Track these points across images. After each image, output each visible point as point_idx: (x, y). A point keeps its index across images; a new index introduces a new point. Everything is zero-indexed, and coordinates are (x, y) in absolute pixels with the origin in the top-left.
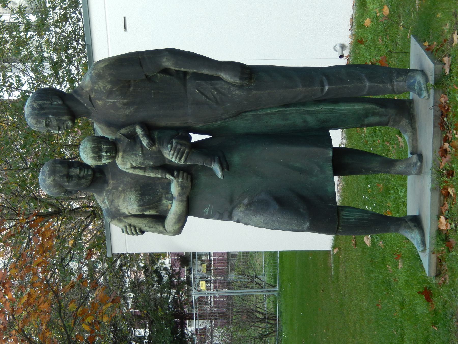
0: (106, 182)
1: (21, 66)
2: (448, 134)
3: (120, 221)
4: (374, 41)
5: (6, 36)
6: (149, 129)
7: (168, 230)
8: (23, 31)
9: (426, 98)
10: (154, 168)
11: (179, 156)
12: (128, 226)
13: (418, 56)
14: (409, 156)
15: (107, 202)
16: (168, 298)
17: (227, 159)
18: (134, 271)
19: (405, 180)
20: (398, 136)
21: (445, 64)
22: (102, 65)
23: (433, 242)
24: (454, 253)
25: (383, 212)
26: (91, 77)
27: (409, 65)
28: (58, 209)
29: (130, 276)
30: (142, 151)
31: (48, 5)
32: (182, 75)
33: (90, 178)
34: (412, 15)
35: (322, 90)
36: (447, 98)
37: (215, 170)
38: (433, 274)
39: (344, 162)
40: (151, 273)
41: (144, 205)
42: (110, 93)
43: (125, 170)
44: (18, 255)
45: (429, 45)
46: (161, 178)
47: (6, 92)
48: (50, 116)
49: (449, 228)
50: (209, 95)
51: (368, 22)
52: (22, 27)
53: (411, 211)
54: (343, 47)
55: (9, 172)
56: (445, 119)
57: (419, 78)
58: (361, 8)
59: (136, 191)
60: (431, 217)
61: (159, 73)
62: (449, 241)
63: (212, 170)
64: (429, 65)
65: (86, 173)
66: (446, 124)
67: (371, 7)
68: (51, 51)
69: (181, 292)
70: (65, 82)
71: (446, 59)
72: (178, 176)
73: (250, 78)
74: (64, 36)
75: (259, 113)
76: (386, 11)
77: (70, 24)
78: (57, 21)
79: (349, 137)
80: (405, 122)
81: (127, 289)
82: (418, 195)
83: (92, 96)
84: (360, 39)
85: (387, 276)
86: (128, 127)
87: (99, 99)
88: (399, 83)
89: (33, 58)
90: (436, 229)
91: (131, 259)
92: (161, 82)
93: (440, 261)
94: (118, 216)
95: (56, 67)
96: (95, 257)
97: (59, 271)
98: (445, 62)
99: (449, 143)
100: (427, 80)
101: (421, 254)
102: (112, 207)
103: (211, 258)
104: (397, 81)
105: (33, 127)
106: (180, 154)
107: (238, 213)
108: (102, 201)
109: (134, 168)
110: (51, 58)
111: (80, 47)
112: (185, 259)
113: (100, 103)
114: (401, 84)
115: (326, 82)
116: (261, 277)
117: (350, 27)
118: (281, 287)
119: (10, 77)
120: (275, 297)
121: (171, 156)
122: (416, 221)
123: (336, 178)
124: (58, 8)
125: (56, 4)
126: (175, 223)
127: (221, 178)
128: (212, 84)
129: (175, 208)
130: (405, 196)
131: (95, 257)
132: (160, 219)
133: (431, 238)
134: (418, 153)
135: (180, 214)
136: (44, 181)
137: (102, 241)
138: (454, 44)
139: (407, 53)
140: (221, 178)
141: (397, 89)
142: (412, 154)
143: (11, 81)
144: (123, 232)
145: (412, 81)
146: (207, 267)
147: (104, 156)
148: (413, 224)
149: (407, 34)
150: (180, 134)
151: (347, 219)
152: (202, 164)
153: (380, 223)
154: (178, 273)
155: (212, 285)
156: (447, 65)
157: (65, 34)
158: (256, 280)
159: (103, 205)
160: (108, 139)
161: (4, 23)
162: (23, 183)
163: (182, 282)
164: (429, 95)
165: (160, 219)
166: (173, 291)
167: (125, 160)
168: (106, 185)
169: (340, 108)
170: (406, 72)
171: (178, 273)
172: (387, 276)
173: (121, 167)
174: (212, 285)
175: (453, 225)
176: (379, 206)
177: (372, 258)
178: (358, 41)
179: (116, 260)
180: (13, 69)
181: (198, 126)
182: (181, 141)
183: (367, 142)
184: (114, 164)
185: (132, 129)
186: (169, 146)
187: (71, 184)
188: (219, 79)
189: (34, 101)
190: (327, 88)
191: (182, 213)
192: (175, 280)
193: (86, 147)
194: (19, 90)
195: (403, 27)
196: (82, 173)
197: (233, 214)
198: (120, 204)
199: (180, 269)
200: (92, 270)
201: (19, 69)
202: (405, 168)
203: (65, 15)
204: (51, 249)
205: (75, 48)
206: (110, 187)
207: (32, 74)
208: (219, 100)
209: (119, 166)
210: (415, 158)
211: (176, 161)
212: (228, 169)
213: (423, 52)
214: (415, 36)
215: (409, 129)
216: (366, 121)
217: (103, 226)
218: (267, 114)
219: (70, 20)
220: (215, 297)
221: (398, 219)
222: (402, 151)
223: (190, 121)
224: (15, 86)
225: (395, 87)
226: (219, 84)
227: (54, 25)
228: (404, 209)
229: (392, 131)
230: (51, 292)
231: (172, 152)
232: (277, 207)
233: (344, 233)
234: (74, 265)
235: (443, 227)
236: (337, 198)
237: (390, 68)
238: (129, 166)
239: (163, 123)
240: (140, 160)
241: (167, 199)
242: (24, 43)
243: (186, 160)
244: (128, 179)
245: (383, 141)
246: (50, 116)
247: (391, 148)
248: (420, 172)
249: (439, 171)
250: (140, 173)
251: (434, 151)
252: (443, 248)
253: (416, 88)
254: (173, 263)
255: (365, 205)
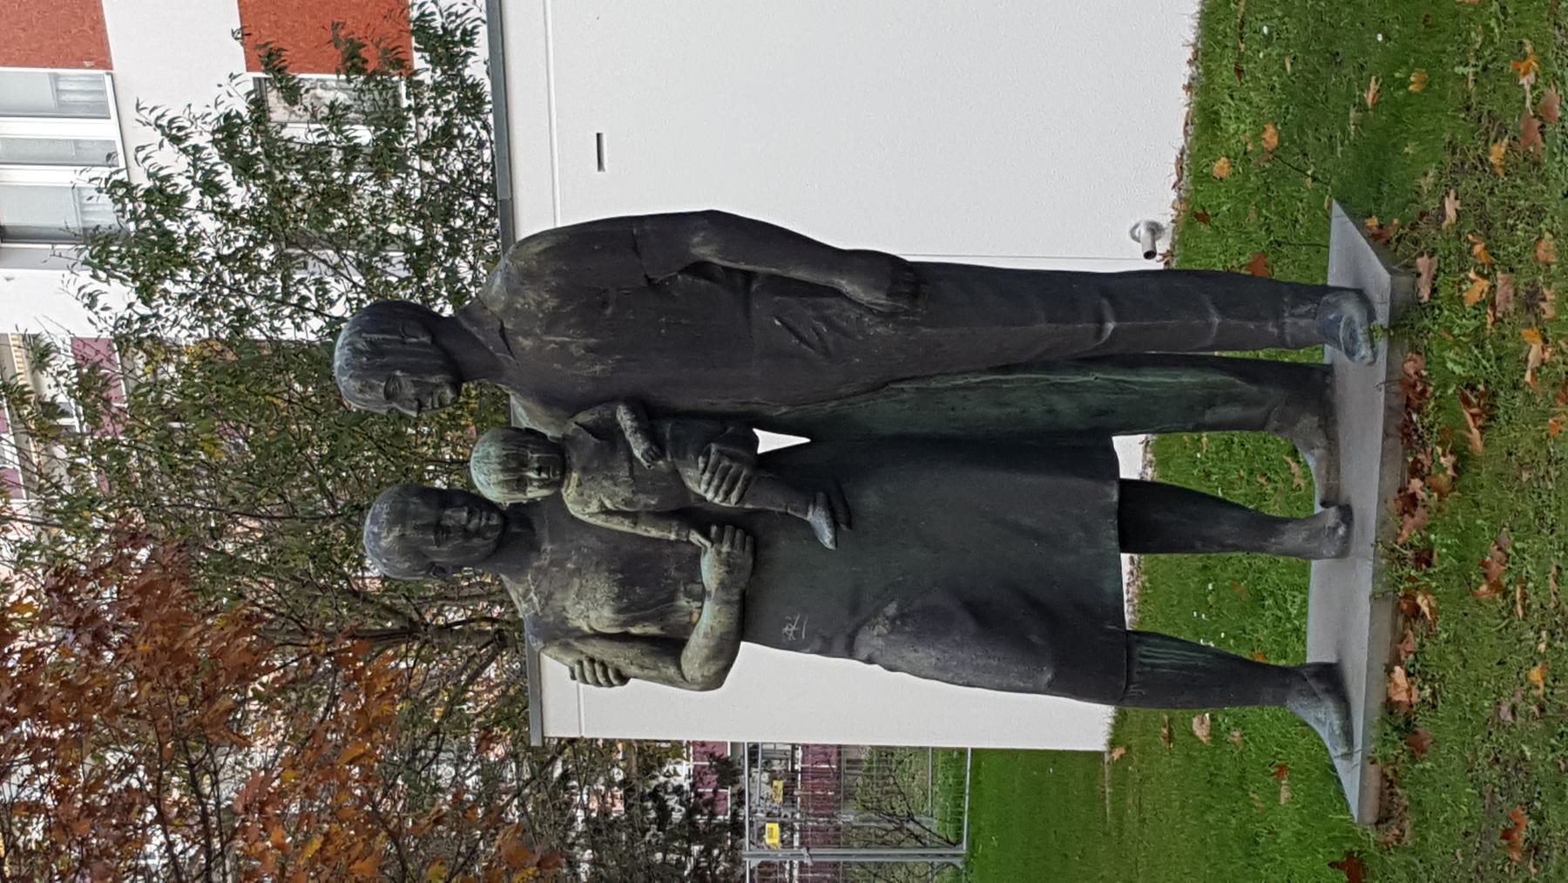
0: (535, 547)
1: (330, 253)
2: (1420, 456)
3: (566, 647)
4: (1233, 213)
5: (293, 176)
6: (649, 415)
7: (689, 678)
8: (339, 166)
9: (1369, 359)
10: (660, 516)
11: (724, 487)
12: (585, 663)
13: (1348, 254)
14: (1318, 509)
15: (535, 599)
16: (680, 865)
17: (849, 500)
18: (597, 792)
19: (1305, 573)
20: (1289, 459)
21: (1419, 275)
22: (536, 248)
23: (1374, 733)
24: (1428, 765)
25: (1245, 654)
26: (507, 279)
27: (1325, 278)
28: (411, 620)
29: (585, 803)
30: (631, 470)
31: (405, 103)
32: (739, 280)
33: (492, 535)
34: (1339, 149)
35: (1100, 331)
36: (1421, 362)
37: (817, 527)
38: (1370, 818)
39: (1147, 517)
40: (643, 798)
41: (629, 608)
42: (552, 322)
43: (585, 518)
44: (303, 736)
45: (1380, 227)
46: (677, 541)
47: (288, 321)
48: (398, 373)
49: (1415, 699)
50: (808, 334)
51: (1221, 167)
52: (337, 157)
53: (1317, 652)
54: (1155, 230)
55: (288, 524)
56: (1415, 417)
57: (1351, 310)
58: (1205, 131)
59: (611, 572)
60: (1369, 669)
61: (680, 272)
62: (1416, 733)
63: (807, 525)
64: (1379, 277)
65: (484, 522)
66: (1416, 430)
67: (1232, 128)
68: (408, 218)
69: (716, 852)
70: (440, 301)
71: (1422, 263)
72: (719, 540)
73: (914, 296)
74: (441, 183)
75: (934, 384)
76: (1271, 137)
77: (459, 153)
78: (426, 144)
79: (1161, 458)
80: (1309, 421)
81: (578, 837)
82: (1338, 612)
83: (508, 326)
84: (1200, 211)
85: (1248, 821)
86: (599, 408)
87: (526, 336)
88: (1297, 322)
89: (361, 237)
90: (1384, 699)
91: (590, 755)
92: (683, 288)
93: (1389, 783)
94: (561, 635)
95: (420, 259)
96: (500, 750)
97: (405, 781)
98: (1421, 270)
99: (1422, 479)
100: (1371, 316)
101: (1339, 764)
102: (548, 611)
103: (798, 767)
104: (1292, 315)
105: (354, 399)
106: (727, 481)
107: (871, 638)
108: (524, 599)
109: (608, 512)
110: (406, 238)
111: (482, 212)
112: (724, 766)
113: (527, 343)
114: (1303, 322)
115: (1108, 312)
116: (923, 819)
117: (1174, 178)
118: (972, 846)
119: (301, 281)
120: (957, 873)
121: (703, 487)
122: (1330, 678)
123: (1125, 557)
124: (430, 110)
125: (426, 101)
126: (708, 659)
127: (831, 547)
128: (815, 307)
129: (709, 619)
130: (1303, 614)
131: (500, 750)
132: (669, 646)
133: (1368, 724)
134: (1342, 502)
135: (721, 638)
136: (377, 537)
137: (519, 705)
138: (1444, 225)
139: (1321, 249)
140: (831, 547)
141: (1293, 337)
142: (1324, 504)
143: (304, 292)
144: (573, 677)
145: (1331, 317)
146: (785, 787)
147: (531, 479)
148: (1323, 686)
149: (1323, 197)
150: (730, 429)
151: (1153, 666)
152: (782, 510)
153: (1235, 679)
154: (711, 803)
155: (797, 836)
156: (1424, 276)
157: (444, 178)
158: (911, 826)
159: (525, 606)
160: (544, 436)
161: (291, 145)
162: (323, 556)
163: (722, 825)
164: (1375, 355)
165: (669, 646)
166: (696, 849)
167: (587, 492)
168: (534, 554)
169: (1143, 379)
170: (1318, 292)
171: (711, 803)
172: (1248, 821)
173: (574, 510)
174: (797, 836)
175: (1427, 691)
176: (1235, 638)
177: (1211, 775)
178: (1194, 215)
179: (554, 759)
180: (311, 262)
181: (775, 414)
182: (731, 450)
183: (1208, 475)
184: (557, 499)
185: (607, 414)
186: (701, 459)
187: (444, 549)
188: (837, 293)
189: (359, 333)
190: (1111, 326)
191: (728, 633)
192: (701, 819)
193: (487, 456)
194: (323, 315)
195: (1315, 180)
196: (475, 521)
197: (857, 643)
198: (568, 604)
199: (715, 792)
200: (490, 776)
201: (324, 261)
202: (1306, 540)
203: (446, 129)
204: (386, 721)
205: (469, 215)
206: (544, 561)
207: (357, 278)
208: (831, 347)
209: (569, 506)
210: (1332, 515)
211: (717, 500)
212: (849, 525)
213: (1363, 241)
214: (1342, 202)
215: (1320, 441)
216: (1209, 416)
217: (522, 673)
218: (955, 388)
219: (459, 142)
220: (802, 864)
221: (1284, 671)
222: (1299, 498)
223: (756, 400)
224: (313, 304)
225: (1288, 330)
226: (833, 307)
227: (419, 153)
228: (1299, 648)
229: (1275, 444)
230: (383, 833)
231: (707, 476)
232: (971, 625)
233: (1140, 701)
234: (446, 772)
235: (1401, 697)
236: (1127, 618)
237: (1278, 282)
238: (594, 507)
239: (686, 402)
240: (624, 492)
241: (690, 595)
242: (341, 197)
243: (741, 499)
244: (593, 541)
245: (1251, 473)
246: (398, 373)
247: (1270, 491)
248: (1343, 553)
249: (1393, 550)
250: (625, 526)
251: (1383, 500)
252: (1398, 750)
253: (1341, 334)
254: (697, 776)
255: (1197, 634)
